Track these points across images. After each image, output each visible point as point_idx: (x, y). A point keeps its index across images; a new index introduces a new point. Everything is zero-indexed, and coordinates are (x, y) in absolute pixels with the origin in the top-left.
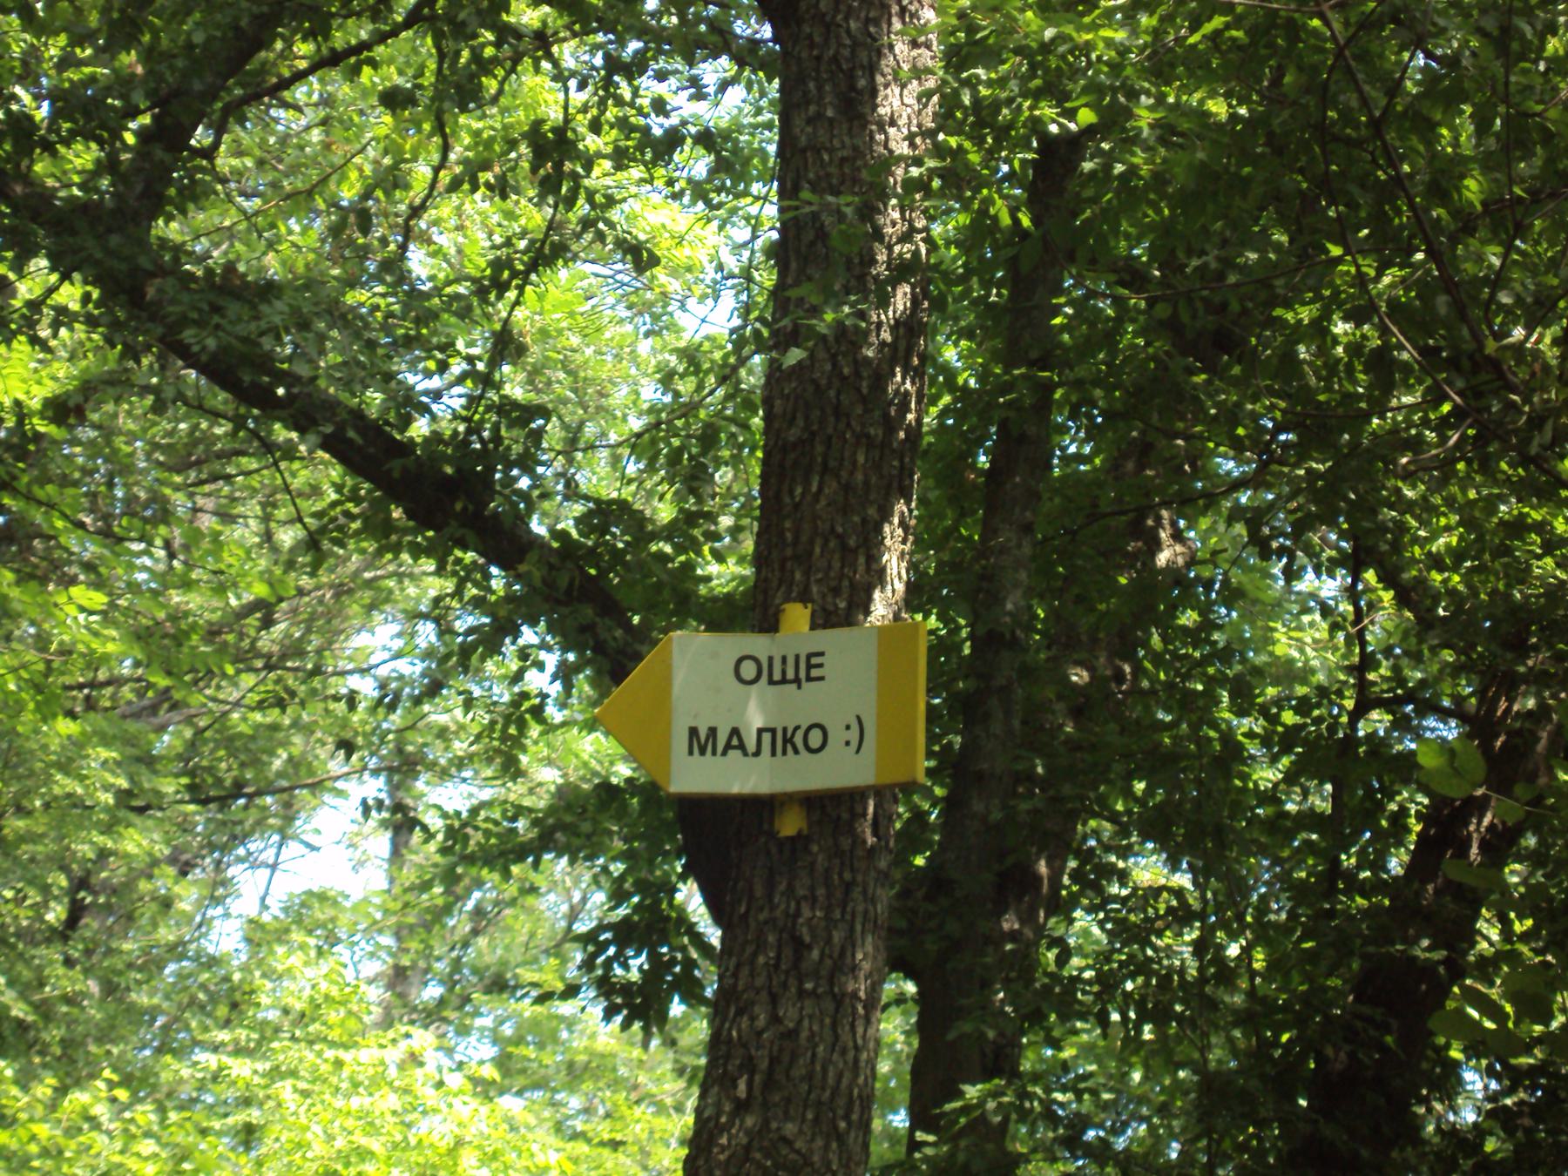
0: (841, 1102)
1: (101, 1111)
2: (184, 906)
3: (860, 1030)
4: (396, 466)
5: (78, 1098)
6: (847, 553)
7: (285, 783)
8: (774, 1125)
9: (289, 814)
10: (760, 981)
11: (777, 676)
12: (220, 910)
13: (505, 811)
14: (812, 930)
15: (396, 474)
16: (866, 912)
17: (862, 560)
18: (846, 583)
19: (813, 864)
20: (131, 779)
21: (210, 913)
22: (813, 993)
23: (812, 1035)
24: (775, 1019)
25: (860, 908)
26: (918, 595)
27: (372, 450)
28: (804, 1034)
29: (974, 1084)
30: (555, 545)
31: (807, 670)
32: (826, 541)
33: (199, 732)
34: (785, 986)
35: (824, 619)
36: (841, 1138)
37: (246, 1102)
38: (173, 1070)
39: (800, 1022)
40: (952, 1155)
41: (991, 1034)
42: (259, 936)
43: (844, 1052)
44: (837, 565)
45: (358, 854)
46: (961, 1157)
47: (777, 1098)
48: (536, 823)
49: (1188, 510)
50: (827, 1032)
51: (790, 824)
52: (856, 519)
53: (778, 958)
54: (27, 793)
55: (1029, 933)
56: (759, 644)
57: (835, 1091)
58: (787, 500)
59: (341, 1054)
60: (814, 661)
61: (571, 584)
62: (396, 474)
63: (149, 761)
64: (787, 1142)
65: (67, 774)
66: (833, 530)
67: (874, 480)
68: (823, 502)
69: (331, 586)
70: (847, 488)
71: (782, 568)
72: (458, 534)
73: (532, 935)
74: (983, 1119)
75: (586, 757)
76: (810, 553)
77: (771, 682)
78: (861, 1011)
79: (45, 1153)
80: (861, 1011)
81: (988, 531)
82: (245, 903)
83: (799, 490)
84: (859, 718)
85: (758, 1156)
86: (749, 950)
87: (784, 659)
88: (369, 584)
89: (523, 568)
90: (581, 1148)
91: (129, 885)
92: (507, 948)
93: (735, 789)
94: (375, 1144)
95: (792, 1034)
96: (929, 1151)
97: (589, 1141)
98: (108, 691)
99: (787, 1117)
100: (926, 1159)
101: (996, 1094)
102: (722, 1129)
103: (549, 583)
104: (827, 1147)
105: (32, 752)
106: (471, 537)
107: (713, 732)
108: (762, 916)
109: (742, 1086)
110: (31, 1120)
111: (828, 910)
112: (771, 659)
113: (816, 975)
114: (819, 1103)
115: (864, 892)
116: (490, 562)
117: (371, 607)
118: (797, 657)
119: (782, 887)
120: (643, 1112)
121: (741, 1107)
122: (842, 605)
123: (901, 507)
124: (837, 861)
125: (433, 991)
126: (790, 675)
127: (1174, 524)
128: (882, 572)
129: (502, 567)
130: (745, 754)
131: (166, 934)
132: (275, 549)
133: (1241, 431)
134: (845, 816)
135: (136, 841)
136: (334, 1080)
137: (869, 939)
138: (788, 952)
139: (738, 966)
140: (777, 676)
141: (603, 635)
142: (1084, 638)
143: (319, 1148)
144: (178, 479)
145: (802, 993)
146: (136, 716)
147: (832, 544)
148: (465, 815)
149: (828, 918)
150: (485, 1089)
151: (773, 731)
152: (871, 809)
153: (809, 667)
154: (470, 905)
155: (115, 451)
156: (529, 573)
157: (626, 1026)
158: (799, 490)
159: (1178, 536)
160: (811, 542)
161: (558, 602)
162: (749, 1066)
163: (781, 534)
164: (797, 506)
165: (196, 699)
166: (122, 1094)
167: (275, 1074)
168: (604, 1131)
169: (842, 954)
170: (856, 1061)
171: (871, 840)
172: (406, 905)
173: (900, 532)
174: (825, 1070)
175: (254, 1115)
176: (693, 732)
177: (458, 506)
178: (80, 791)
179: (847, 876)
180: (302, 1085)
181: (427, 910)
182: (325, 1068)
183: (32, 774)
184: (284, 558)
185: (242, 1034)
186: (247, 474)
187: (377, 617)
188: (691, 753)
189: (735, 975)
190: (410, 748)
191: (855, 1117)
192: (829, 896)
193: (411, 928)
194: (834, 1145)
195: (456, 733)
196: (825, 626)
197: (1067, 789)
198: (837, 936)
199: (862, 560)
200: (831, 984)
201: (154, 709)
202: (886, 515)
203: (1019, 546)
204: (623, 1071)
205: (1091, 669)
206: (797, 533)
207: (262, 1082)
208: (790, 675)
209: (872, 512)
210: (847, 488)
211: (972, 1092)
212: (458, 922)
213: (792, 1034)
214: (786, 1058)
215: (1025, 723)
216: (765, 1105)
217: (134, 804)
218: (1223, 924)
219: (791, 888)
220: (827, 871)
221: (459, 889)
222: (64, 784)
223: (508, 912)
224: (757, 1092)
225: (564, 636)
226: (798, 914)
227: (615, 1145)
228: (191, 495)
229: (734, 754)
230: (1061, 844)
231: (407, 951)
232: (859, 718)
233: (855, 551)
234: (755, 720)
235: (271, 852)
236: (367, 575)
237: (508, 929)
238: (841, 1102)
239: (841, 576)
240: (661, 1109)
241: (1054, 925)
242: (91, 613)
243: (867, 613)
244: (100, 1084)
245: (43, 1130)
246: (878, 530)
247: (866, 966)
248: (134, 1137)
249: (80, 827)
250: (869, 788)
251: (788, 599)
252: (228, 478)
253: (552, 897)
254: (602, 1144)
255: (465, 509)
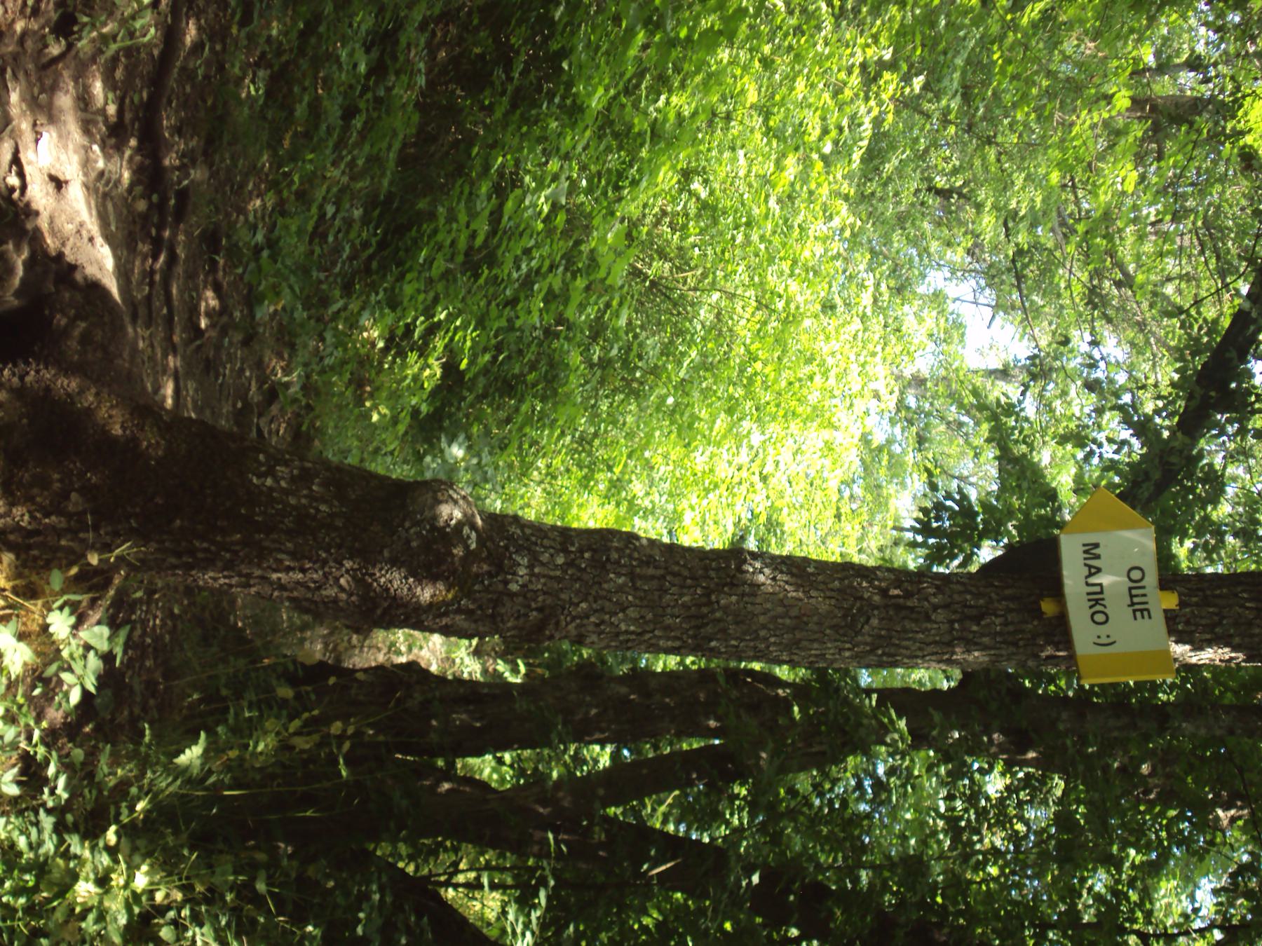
0: (893, 650)
1: (836, 223)
2: (949, 253)
3: (934, 658)
4: (1233, 354)
5: (843, 207)
6: (1211, 628)
7: (1027, 304)
8: (876, 612)
9: (1009, 308)
10: (956, 597)
11: (1134, 592)
12: (949, 275)
13: (1029, 436)
14: (988, 625)
15: (1228, 355)
16: (1002, 656)
17: (1208, 636)
18: (1193, 628)
19: (1027, 623)
20: (1023, 217)
21: (946, 269)
22: (953, 629)
23: (929, 630)
24: (935, 608)
25: (1004, 652)
26: (1190, 670)
27: (1241, 339)
28: (929, 626)
29: (907, 725)
30: (1195, 452)
31: (1139, 610)
32: (1216, 614)
33: (1051, 252)
34: (955, 612)
35: (1170, 617)
36: (872, 651)
37: (847, 305)
38: (862, 260)
39: (936, 622)
40: (867, 716)
41: (935, 733)
42: (937, 297)
43: (920, 649)
44: (1203, 622)
45: (986, 351)
46: (865, 721)
47: (891, 613)
48: (1024, 455)
49: (1250, 827)
50: (931, 639)
51: (1048, 607)
52: (1232, 631)
53: (971, 607)
54: (1011, 158)
55: (993, 750)
56: (1151, 579)
57: (898, 646)
58: (1239, 589)
59: (880, 355)
60: (1146, 613)
61: (1173, 464)
62: (1228, 355)
63: (1033, 225)
64: (867, 622)
65: (1025, 180)
66: (1224, 617)
67: (1256, 639)
68: (1240, 610)
69: (1144, 320)
70: (1250, 624)
71: (1198, 589)
72: (1197, 396)
73: (949, 456)
74: (887, 732)
75: (1058, 478)
76: (1209, 606)
77: (1130, 589)
78: (946, 657)
79: (811, 193)
80: (946, 657)
81: (1228, 709)
82: (952, 290)
83: (1245, 595)
84: (1114, 643)
85: (858, 604)
86: (973, 589)
87: (1144, 595)
88: (1147, 342)
89: (1179, 434)
90: (835, 497)
91: (961, 223)
92: (940, 443)
93: (1065, 573)
94: (832, 381)
95: (928, 619)
96: (867, 701)
97: (839, 500)
98: (1072, 198)
99: (881, 619)
100: (862, 701)
101: (902, 738)
102: (871, 582)
103: (1172, 451)
104: (866, 644)
105: (1036, 158)
106: (1194, 403)
107: (1098, 557)
108: (993, 595)
109: (896, 592)
110: (830, 183)
111: (1000, 634)
112: (1143, 587)
113: (963, 629)
114: (891, 638)
115: (1014, 654)
116: (1181, 416)
117: (1133, 344)
118: (1146, 603)
119: (1012, 606)
120: (857, 533)
121: (884, 592)
122: (1180, 627)
123: (1241, 656)
124: (1029, 636)
125: (911, 401)
126: (1136, 600)
127: (1240, 818)
128: (1201, 649)
129: (1178, 423)
130: (1087, 577)
131: (934, 246)
132: (1163, 284)
133: (702, 696)
134: (1056, 639)
135: (988, 223)
136: (865, 353)
137: (987, 659)
138: (974, 612)
139: (963, 584)
140: (1134, 592)
141: (1145, 486)
142: (1168, 770)
143: (826, 349)
144: (1199, 223)
145: (951, 622)
146: (1059, 214)
147: (1216, 618)
148: (1023, 414)
149: (996, 633)
150: (865, 439)
151: (1101, 592)
152: (1061, 654)
153: (1142, 611)
154: (965, 419)
155: (1212, 185)
156: (1177, 439)
157: (917, 520)
158: (1245, 595)
159: (1233, 820)
160: (1215, 606)
161: (1161, 457)
162: (908, 595)
163: (1219, 587)
164: (1236, 595)
165: (1070, 249)
166: (847, 234)
167: (864, 318)
168: (845, 509)
169: (976, 644)
170: (917, 657)
171: (1043, 655)
172: (962, 382)
173: (1227, 657)
174: (909, 639)
175: (840, 309)
176: (1096, 546)
177: (1213, 394)
178: (1016, 189)
179: (1021, 643)
180: (860, 334)
181: (960, 395)
182: (870, 347)
183: (1023, 159)
184: (1159, 289)
185: (886, 297)
186: (1206, 263)
187: (1127, 348)
188: (1084, 545)
189: (958, 582)
190: (1054, 376)
191: (885, 658)
192: (1008, 633)
193: (949, 386)
194: (868, 648)
195: (1065, 401)
196: (1166, 618)
197: (1081, 768)
198: (986, 640)
199: (1208, 636)
200: (959, 639)
201: (1063, 224)
202: (1234, 649)
203: (1220, 727)
204: (879, 517)
205: (1150, 775)
206: (1219, 596)
207: (860, 313)
208: (1136, 600)
209: (1237, 640)
210: (1250, 624)
211: (902, 724)
212: (953, 413)
213: (928, 619)
214: (914, 616)
215: (1116, 738)
216: (886, 606)
217: (1009, 220)
218: (1007, 864)
219: (1010, 610)
220: (1022, 631)
221: (974, 412)
222: (1019, 179)
223: (961, 441)
224: (893, 601)
225: (1140, 463)
226: (997, 616)
227: (838, 516)
228: (1190, 232)
229: (1086, 571)
230: (1047, 765)
231: (936, 385)
232: (1114, 643)
233: (1212, 632)
234: (1105, 579)
235: (985, 301)
236: (1152, 340)
237: (951, 442)
238: (893, 650)
239: (1197, 625)
240: (861, 539)
241: (999, 767)
242: (1122, 184)
243: (1177, 642)
244: (852, 219)
245: (824, 191)
246: (1226, 646)
247: (971, 658)
248: (824, 243)
249: (995, 190)
250: (1075, 652)
251: (1180, 595)
252: (1202, 252)
253: (971, 465)
254: (838, 509)
255: (1211, 397)
